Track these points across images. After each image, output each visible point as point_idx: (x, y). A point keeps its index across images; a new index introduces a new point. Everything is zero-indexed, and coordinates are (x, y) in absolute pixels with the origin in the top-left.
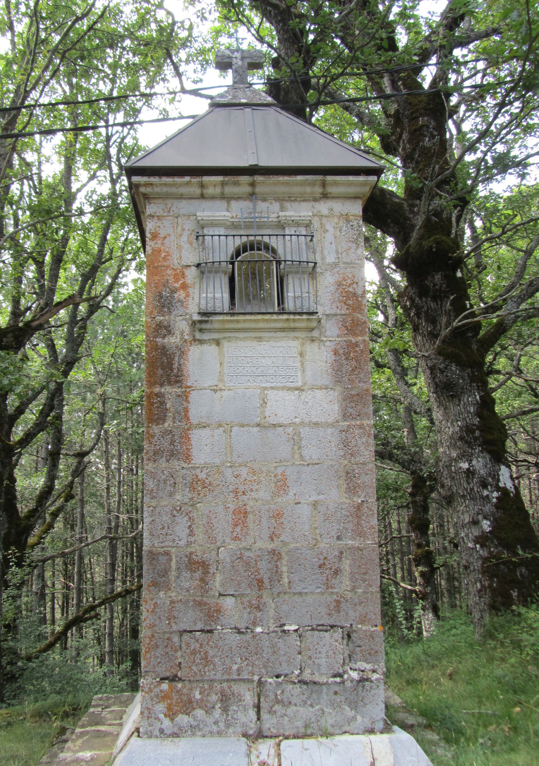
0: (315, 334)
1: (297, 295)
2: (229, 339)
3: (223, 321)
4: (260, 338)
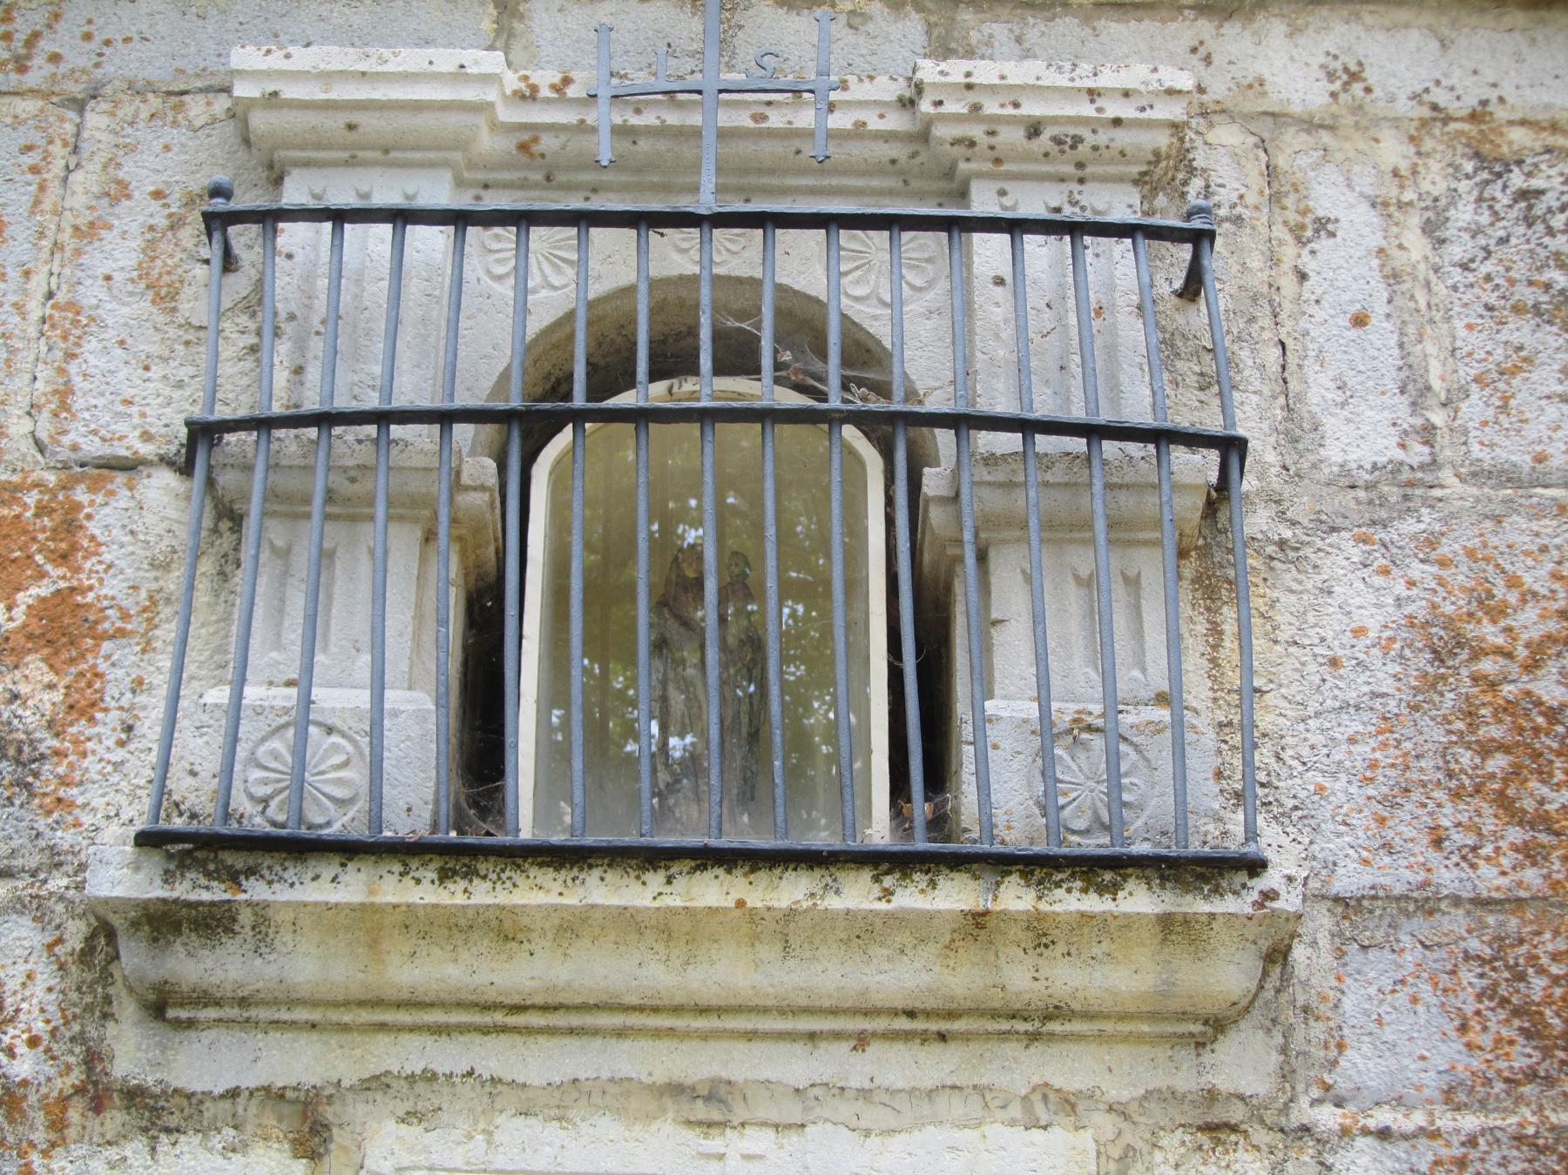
0: (1243, 1066)
1: (1064, 712)
2: (418, 1098)
3: (368, 922)
4: (716, 1093)
